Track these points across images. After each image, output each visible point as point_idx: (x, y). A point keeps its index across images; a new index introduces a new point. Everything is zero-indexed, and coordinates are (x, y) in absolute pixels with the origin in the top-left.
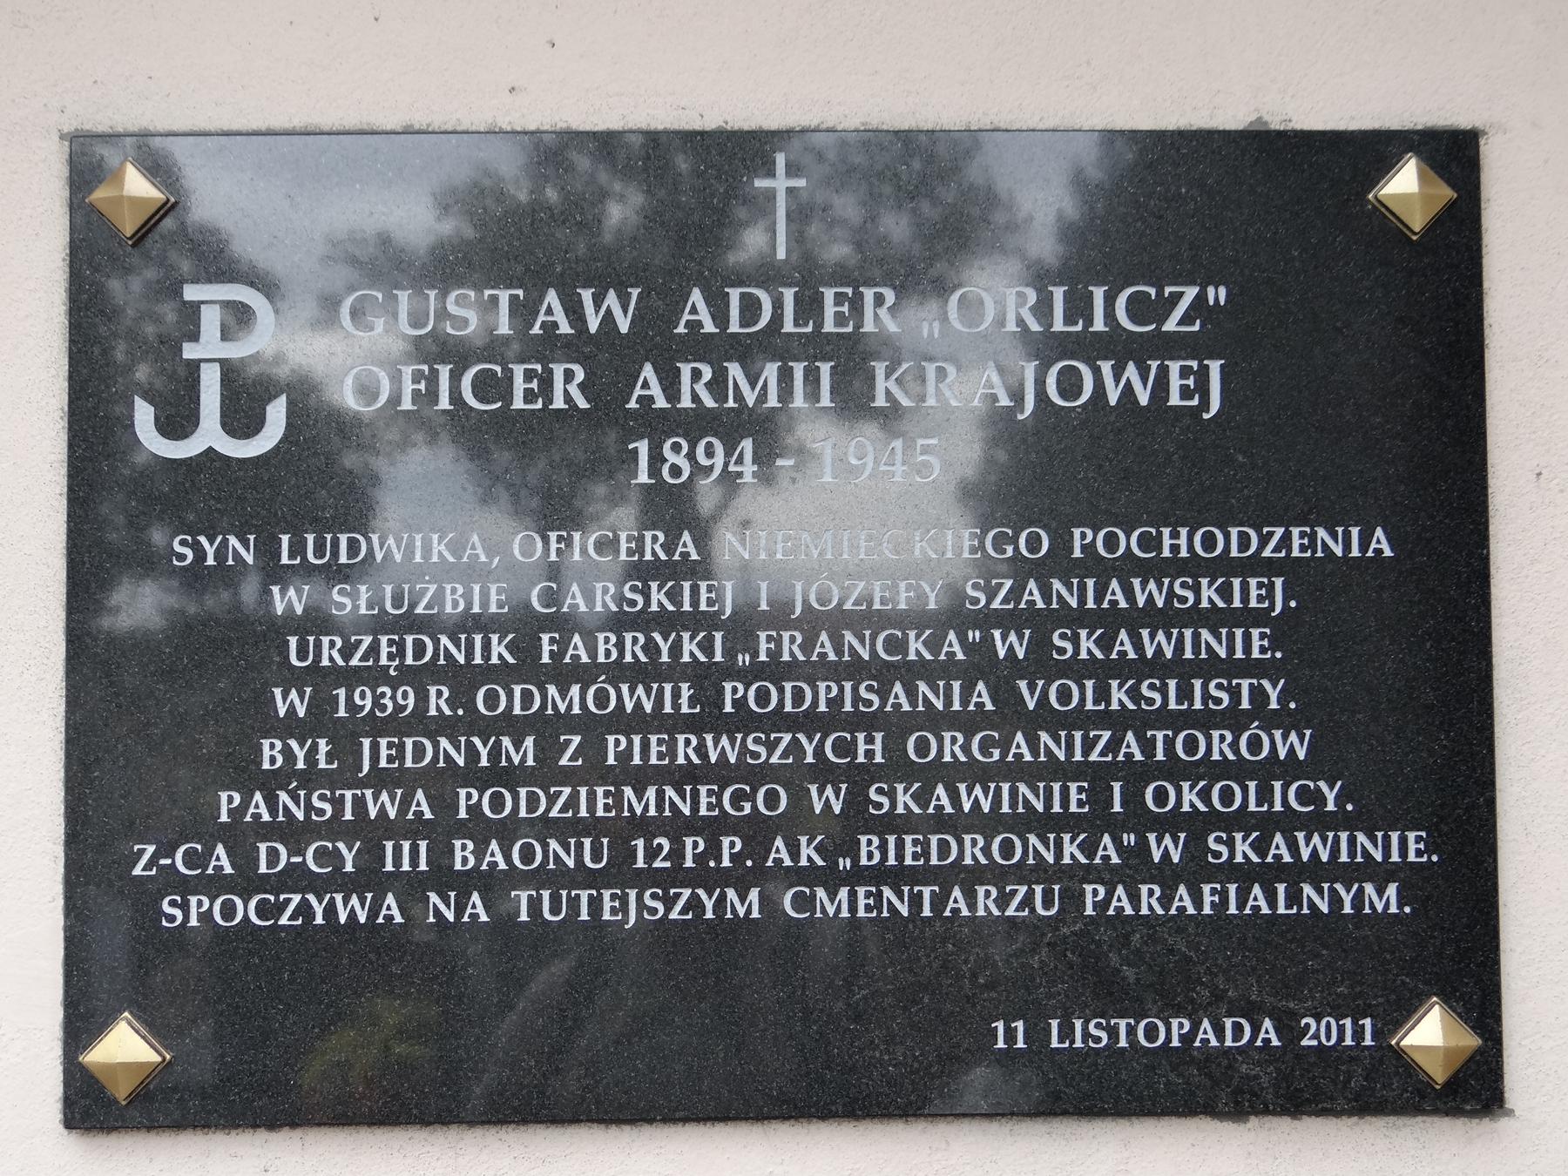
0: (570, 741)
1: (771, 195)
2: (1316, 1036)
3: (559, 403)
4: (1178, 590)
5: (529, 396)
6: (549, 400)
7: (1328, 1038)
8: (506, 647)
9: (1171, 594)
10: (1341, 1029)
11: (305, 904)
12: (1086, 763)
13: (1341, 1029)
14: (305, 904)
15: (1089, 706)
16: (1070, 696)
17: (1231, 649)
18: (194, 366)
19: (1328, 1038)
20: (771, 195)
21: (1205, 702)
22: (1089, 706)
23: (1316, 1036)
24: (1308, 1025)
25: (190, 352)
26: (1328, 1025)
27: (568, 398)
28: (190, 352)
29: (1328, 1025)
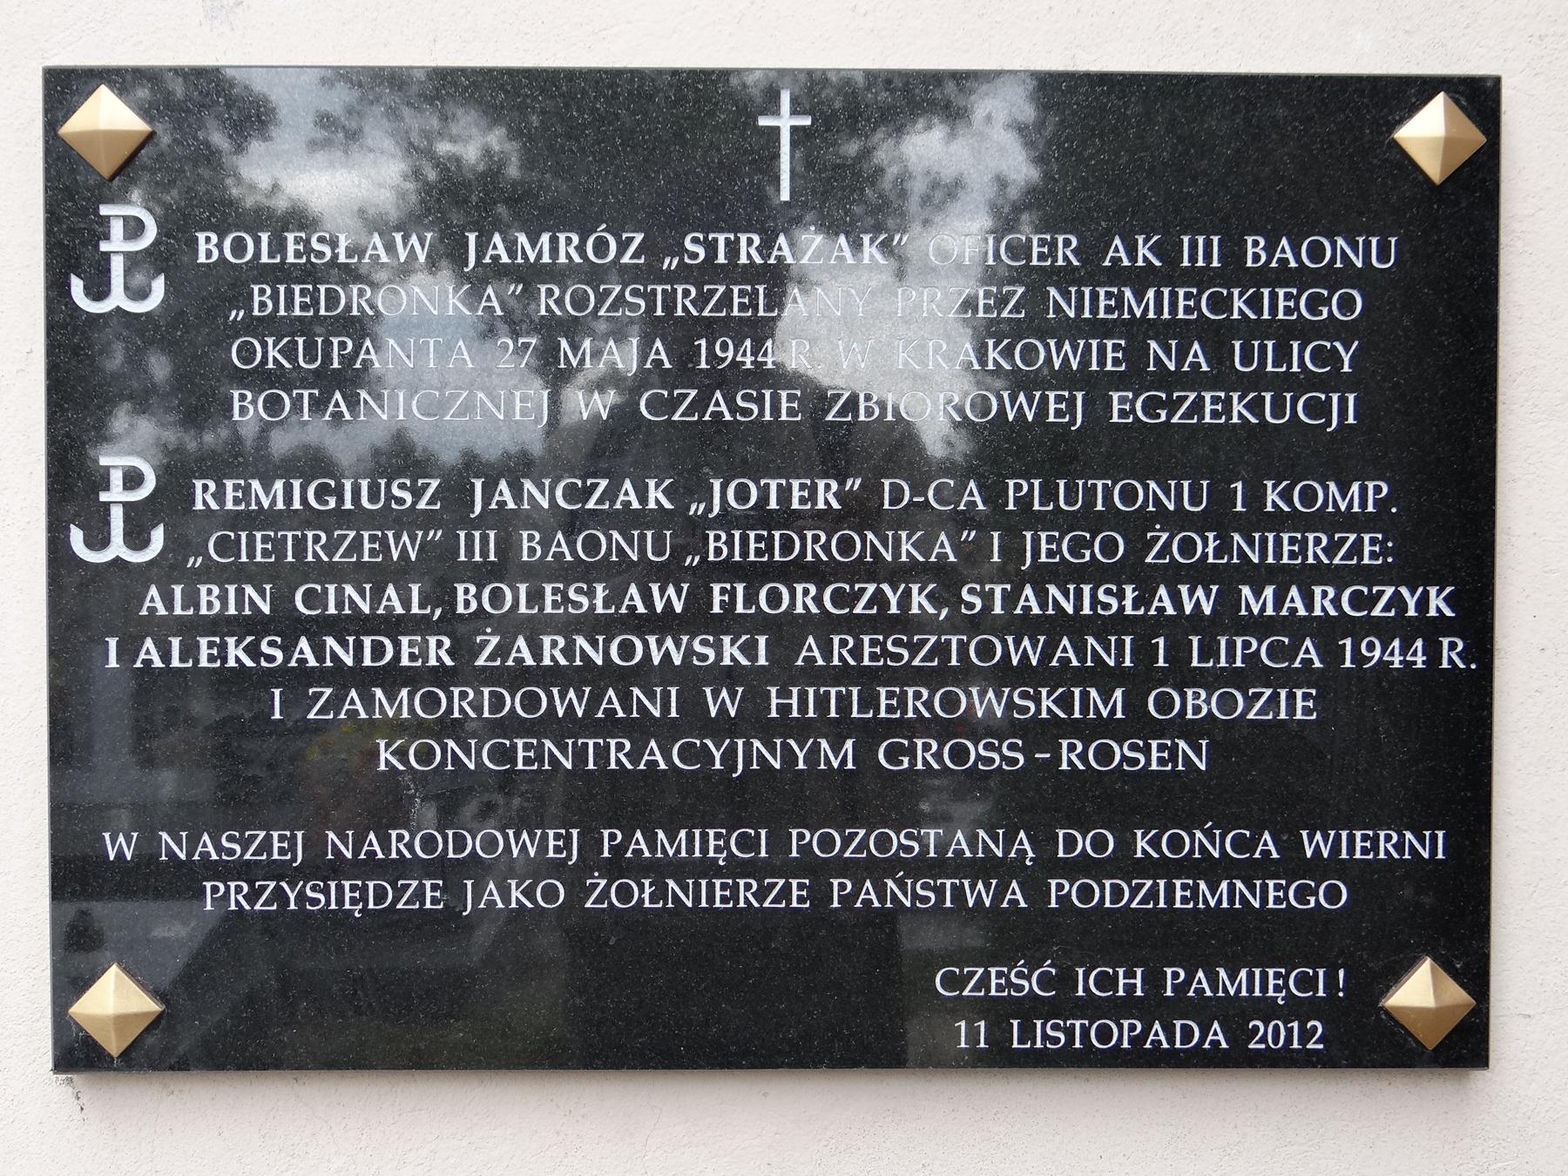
0: (864, 590)
1: (794, 112)
2: (1264, 1040)
3: (821, 505)
4: (698, 647)
5: (802, 501)
6: (815, 503)
7: (1276, 1041)
8: (1445, 599)
9: (689, 652)
10: (1290, 1031)
11: (879, 593)
12: (1154, 878)
13: (1290, 1031)
14: (879, 593)
15: (265, 259)
16: (245, 248)
17: (240, 593)
18: (107, 256)
19: (1276, 1041)
20: (794, 112)
21: (1093, 607)
22: (265, 259)
23: (1264, 1040)
24: (1256, 1028)
25: (104, 247)
26: (1276, 1028)
27: (827, 502)
28: (104, 247)
29: (1276, 1028)
